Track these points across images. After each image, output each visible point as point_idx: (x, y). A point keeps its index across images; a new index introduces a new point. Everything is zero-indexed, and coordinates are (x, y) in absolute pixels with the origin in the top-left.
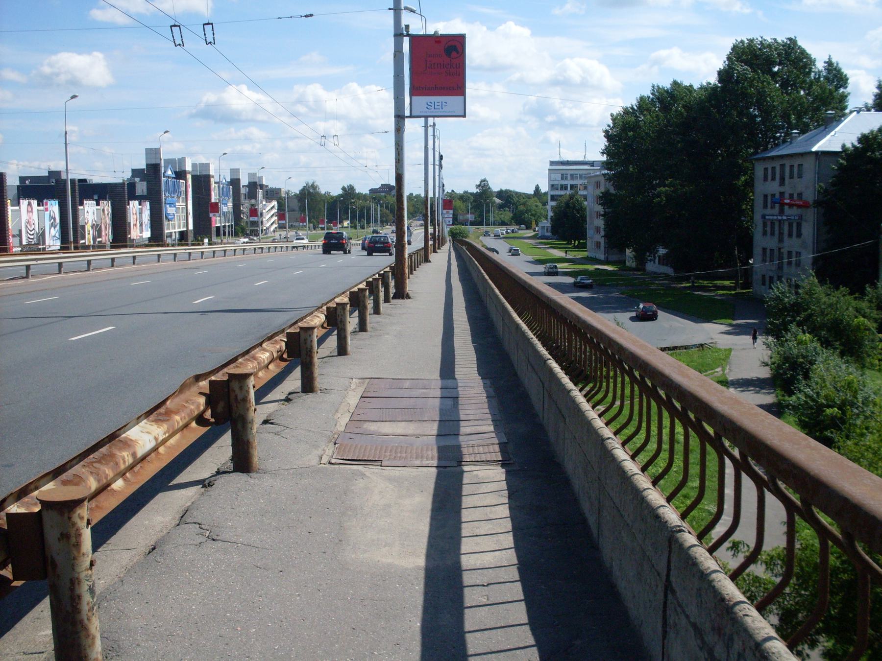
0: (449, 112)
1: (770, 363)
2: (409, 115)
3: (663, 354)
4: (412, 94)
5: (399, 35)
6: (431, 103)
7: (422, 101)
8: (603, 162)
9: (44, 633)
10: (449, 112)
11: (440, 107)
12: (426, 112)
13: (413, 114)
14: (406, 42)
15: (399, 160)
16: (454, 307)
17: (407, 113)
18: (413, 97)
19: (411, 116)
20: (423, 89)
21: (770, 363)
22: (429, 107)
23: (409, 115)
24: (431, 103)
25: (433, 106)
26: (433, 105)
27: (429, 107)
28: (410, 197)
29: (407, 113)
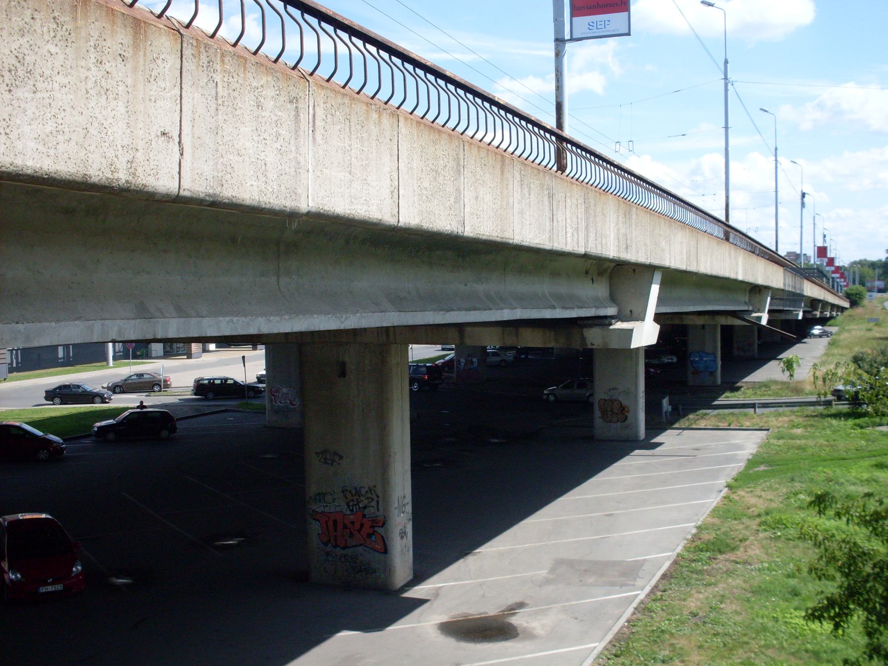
0: (613, 31)
1: (705, 603)
2: (569, 38)
3: (517, 599)
4: (573, 15)
5: (815, 246)
6: (593, 22)
7: (583, 22)
8: (878, 657)
9: (435, 465)
10: (613, 31)
11: (603, 26)
12: (587, 33)
13: (574, 37)
14: (816, 248)
15: (558, 87)
16: (477, 321)
17: (567, 37)
18: (574, 19)
19: (572, 39)
20: (584, 9)
21: (705, 603)
22: (591, 27)
23: (569, 38)
24: (593, 22)
25: (595, 27)
26: (595, 25)
27: (591, 27)
28: (216, 348)
29: (567, 37)
